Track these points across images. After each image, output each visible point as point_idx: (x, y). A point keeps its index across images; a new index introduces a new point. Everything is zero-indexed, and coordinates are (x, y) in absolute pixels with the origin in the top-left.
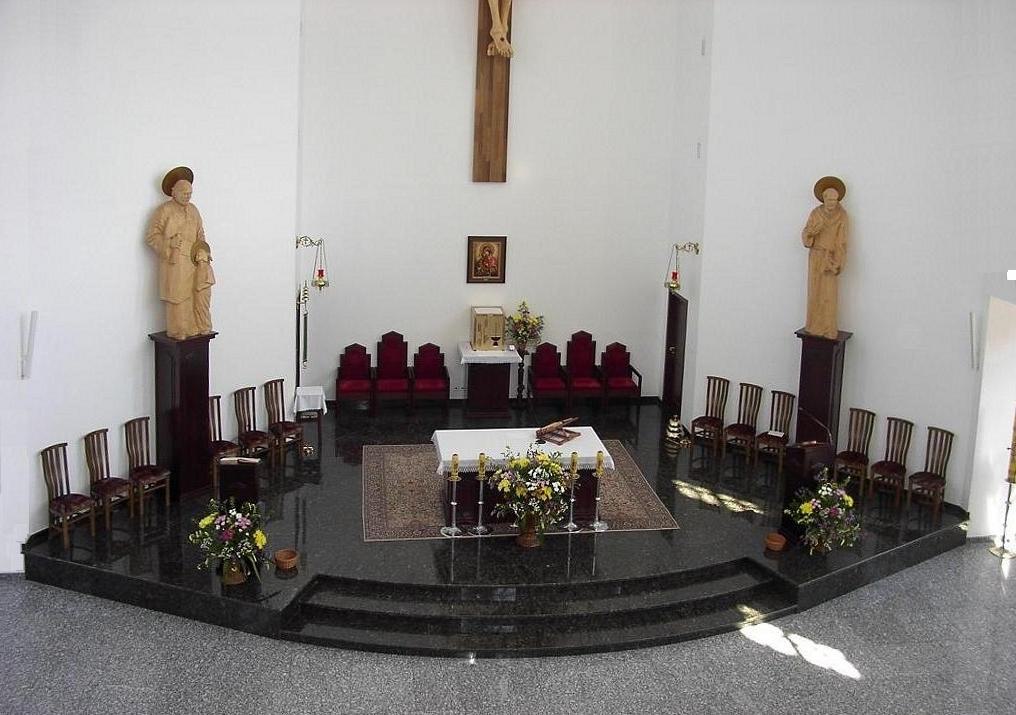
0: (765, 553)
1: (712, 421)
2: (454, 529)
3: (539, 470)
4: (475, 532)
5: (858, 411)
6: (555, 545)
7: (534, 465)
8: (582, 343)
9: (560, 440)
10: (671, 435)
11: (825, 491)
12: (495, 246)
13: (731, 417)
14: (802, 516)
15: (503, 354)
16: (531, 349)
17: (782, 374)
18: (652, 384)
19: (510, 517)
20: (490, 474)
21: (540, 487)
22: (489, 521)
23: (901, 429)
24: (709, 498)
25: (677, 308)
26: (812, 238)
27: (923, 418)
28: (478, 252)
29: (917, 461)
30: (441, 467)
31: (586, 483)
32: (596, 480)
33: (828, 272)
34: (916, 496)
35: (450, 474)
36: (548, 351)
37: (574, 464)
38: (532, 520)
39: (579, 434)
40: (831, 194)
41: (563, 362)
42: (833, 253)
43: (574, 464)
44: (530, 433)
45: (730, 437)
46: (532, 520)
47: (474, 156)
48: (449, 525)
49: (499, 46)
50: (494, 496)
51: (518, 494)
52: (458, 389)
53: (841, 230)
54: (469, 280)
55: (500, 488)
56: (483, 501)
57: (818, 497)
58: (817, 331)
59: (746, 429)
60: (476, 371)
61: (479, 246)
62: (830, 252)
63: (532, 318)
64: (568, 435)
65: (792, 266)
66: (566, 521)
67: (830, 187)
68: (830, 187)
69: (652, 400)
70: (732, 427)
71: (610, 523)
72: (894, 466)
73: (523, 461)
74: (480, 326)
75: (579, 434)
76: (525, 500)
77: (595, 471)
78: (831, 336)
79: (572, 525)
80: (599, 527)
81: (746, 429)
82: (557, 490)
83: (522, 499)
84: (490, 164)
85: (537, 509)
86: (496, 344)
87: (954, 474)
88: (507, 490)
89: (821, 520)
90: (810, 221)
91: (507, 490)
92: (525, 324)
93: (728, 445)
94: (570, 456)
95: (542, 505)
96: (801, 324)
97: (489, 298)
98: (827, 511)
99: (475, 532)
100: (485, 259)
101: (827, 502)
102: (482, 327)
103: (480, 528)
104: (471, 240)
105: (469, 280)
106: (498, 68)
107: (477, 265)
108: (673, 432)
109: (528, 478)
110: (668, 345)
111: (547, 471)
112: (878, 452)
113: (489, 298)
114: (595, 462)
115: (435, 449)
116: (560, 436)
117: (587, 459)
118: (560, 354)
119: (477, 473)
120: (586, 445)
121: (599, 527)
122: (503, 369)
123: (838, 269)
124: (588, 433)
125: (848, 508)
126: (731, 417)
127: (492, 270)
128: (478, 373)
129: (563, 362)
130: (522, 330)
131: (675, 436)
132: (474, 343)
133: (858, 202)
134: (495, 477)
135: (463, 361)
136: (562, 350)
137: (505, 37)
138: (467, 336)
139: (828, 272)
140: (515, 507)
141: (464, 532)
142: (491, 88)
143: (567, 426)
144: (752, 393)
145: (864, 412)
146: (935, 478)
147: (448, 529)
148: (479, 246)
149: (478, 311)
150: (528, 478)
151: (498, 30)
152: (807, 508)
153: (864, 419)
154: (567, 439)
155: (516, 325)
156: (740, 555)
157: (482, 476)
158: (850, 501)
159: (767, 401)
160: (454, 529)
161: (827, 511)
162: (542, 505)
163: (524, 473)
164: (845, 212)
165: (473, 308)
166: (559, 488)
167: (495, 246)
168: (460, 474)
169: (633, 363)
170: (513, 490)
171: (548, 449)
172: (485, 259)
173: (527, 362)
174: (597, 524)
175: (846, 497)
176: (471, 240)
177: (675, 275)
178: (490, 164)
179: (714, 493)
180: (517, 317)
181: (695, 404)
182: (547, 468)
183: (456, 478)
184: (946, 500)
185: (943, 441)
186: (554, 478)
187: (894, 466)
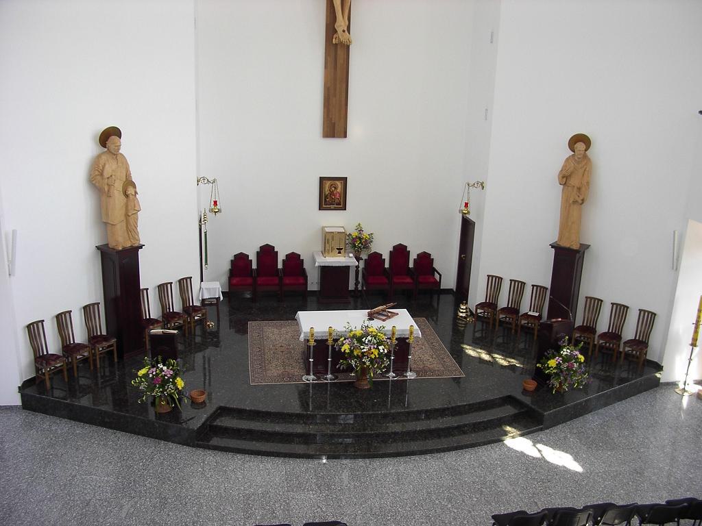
1: (490, 305)
2: (312, 377)
3: (369, 338)
4: (326, 379)
5: (591, 298)
7: (366, 335)
8: (400, 252)
9: (384, 318)
10: (461, 314)
11: (565, 352)
12: (339, 184)
13: (503, 302)
14: (549, 368)
16: (364, 256)
17: (539, 273)
18: (449, 280)
19: (350, 369)
20: (336, 340)
21: (370, 349)
23: (620, 310)
25: (467, 227)
26: (565, 178)
27: (635, 303)
28: (327, 188)
31: (402, 347)
33: (575, 202)
35: (308, 341)
36: (376, 257)
37: (393, 334)
38: (364, 371)
39: (397, 314)
40: (580, 146)
41: (387, 265)
42: (579, 189)
43: (393, 334)
45: (501, 316)
46: (364, 371)
47: (324, 118)
48: (308, 374)
49: (341, 36)
50: (338, 355)
51: (355, 353)
52: (313, 283)
53: (586, 172)
55: (343, 350)
57: (561, 356)
59: (513, 310)
60: (326, 271)
61: (327, 184)
63: (365, 235)
64: (389, 314)
65: (551, 197)
67: (581, 141)
68: (581, 141)
69: (448, 291)
70: (503, 309)
71: (418, 373)
72: (614, 336)
73: (359, 332)
74: (328, 240)
75: (397, 314)
76: (360, 358)
77: (408, 338)
78: (575, 247)
79: (392, 374)
80: (410, 375)
81: (513, 310)
82: (382, 351)
85: (368, 363)
86: (339, 253)
87: (655, 341)
88: (347, 351)
91: (347, 351)
92: (360, 239)
95: (372, 361)
96: (554, 238)
97: (334, 220)
99: (326, 379)
100: (332, 193)
101: (567, 359)
102: (330, 241)
104: (322, 180)
106: (340, 52)
107: (326, 197)
108: (462, 312)
109: (362, 343)
111: (375, 338)
112: (603, 326)
113: (334, 220)
114: (408, 332)
115: (298, 324)
117: (403, 330)
119: (327, 340)
120: (402, 322)
121: (410, 375)
122: (346, 269)
124: (403, 313)
125: (580, 363)
126: (503, 302)
127: (337, 201)
128: (332, 275)
129: (387, 265)
130: (358, 243)
131: (464, 315)
133: (599, 153)
134: (340, 343)
135: (317, 264)
136: (386, 256)
137: (346, 29)
138: (320, 247)
139: (575, 202)
140: (353, 363)
141: (319, 378)
144: (518, 286)
146: (641, 343)
147: (307, 377)
148: (327, 184)
149: (327, 230)
150: (362, 343)
151: (341, 24)
152: (552, 363)
153: (595, 304)
154: (389, 317)
155: (354, 240)
157: (330, 342)
158: (582, 358)
159: (528, 291)
160: (312, 377)
162: (372, 361)
163: (359, 340)
164: (589, 159)
165: (323, 228)
166: (383, 350)
168: (315, 341)
170: (352, 351)
172: (332, 193)
174: (409, 374)
175: (580, 356)
176: (322, 180)
177: (466, 205)
180: (355, 234)
181: (478, 293)
182: (375, 337)
183: (312, 343)
184: (648, 358)
185: (648, 319)
187: (614, 336)
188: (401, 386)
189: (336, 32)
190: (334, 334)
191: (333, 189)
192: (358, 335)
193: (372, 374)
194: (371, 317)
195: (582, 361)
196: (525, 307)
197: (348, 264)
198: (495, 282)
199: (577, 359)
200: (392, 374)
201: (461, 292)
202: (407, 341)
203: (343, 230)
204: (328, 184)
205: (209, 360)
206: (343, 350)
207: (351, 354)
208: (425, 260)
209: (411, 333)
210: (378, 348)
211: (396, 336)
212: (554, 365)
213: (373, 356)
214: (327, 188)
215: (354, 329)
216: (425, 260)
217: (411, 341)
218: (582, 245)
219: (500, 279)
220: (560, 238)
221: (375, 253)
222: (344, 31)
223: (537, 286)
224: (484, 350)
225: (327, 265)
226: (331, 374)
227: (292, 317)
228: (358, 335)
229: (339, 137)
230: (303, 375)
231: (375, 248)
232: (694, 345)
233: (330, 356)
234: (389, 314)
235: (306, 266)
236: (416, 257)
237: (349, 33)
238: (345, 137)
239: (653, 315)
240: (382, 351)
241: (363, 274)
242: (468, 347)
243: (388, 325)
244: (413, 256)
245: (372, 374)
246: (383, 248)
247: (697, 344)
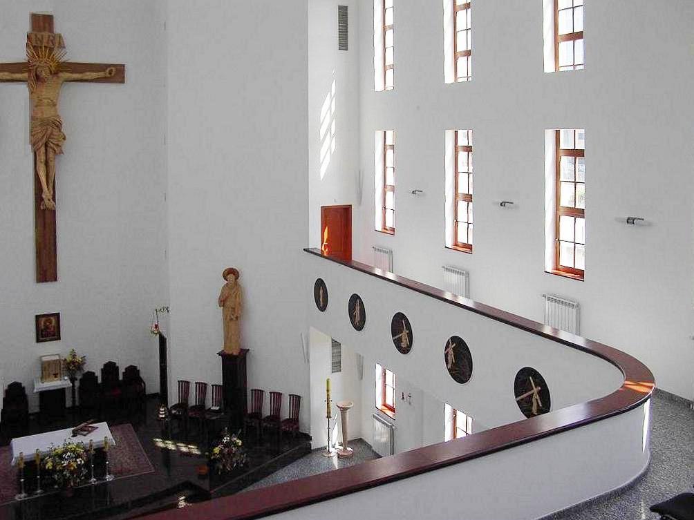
0: (199, 478)
1: (182, 405)
2: (23, 495)
3: (69, 454)
6: (78, 492)
7: (65, 452)
8: (110, 368)
9: (85, 433)
10: (161, 416)
11: (225, 440)
12: (53, 320)
13: (192, 401)
14: (214, 454)
15: (62, 382)
16: (79, 377)
17: (213, 375)
18: (153, 386)
19: (55, 482)
20: (42, 460)
21: (69, 463)
22: (44, 487)
23: (277, 396)
24: (184, 449)
26: (223, 302)
27: (286, 390)
28: (42, 323)
29: (285, 413)
31: (98, 456)
32: (105, 452)
34: (285, 432)
36: (91, 375)
37: (91, 446)
38: (67, 481)
40: (231, 277)
41: (100, 381)
42: (233, 309)
43: (91, 446)
44: (68, 432)
45: (190, 414)
46: (67, 481)
48: (20, 493)
49: (48, 203)
52: (34, 406)
54: (38, 341)
55: (47, 467)
56: (40, 475)
57: (222, 443)
58: (228, 352)
59: (201, 407)
60: (43, 394)
61: (43, 321)
63: (78, 359)
64: (90, 429)
65: (216, 314)
66: (88, 477)
67: (231, 273)
69: (154, 395)
70: (192, 407)
71: (115, 474)
72: (275, 417)
73: (60, 451)
74: (45, 368)
76: (61, 471)
79: (93, 479)
80: (109, 478)
81: (201, 407)
82: (79, 463)
84: (46, 270)
85: (68, 475)
86: (56, 377)
87: (303, 416)
89: (224, 455)
93: (190, 418)
94: (103, 439)
96: (220, 348)
97: (52, 350)
98: (227, 450)
100: (47, 327)
101: (227, 445)
102: (48, 369)
104: (37, 317)
105: (38, 341)
106: (48, 214)
107: (42, 331)
108: (162, 414)
111: (74, 454)
112: (267, 411)
114: (103, 443)
115: (11, 449)
116: (85, 431)
118: (97, 377)
119: (35, 461)
120: (101, 433)
121: (109, 478)
122: (61, 391)
124: (103, 426)
125: (238, 447)
127: (52, 333)
130: (72, 366)
131: (163, 416)
133: (246, 279)
134: (44, 461)
135: (35, 391)
136: (98, 374)
137: (51, 198)
138: (39, 374)
141: (29, 495)
142: (45, 227)
143: (91, 423)
144: (202, 387)
145: (258, 390)
146: (295, 420)
148: (43, 321)
149: (44, 359)
151: (46, 194)
152: (217, 450)
153: (259, 394)
154: (90, 432)
156: (184, 479)
157: (38, 462)
158: (240, 442)
159: (209, 390)
160: (23, 495)
161: (227, 450)
162: (72, 473)
163: (60, 456)
164: (240, 285)
166: (81, 461)
167: (53, 320)
168: (25, 463)
169: (141, 375)
172: (47, 327)
174: (108, 477)
175: (238, 441)
176: (37, 317)
178: (46, 270)
180: (69, 359)
181: (174, 398)
182: (73, 452)
185: (296, 400)
186: (78, 456)
187: (275, 417)
188: (103, 489)
190: (40, 454)
191: (48, 324)
193: (72, 484)
194: (75, 434)
195: (240, 444)
196: (211, 404)
197: (63, 387)
198: (185, 385)
199: (235, 444)
200: (93, 479)
201: (163, 396)
202: (104, 450)
203: (57, 358)
204: (43, 319)
205: (305, 361)
206: (47, 467)
207: (54, 470)
208: (132, 372)
210: (76, 461)
214: (42, 323)
215: (57, 448)
216: (132, 372)
218: (242, 350)
227: (7, 443)
231: (86, 369)
232: (329, 417)
234: (90, 429)
235: (27, 392)
236: (124, 371)
239: (299, 397)
241: (79, 392)
246: (95, 366)
247: (331, 416)
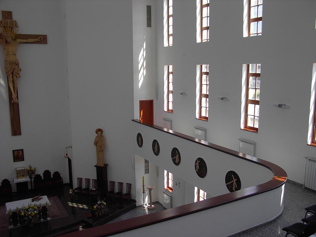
1: (80, 188)
2: (12, 226)
3: (31, 209)
4: (18, 226)
5: (111, 182)
7: (29, 208)
8: (47, 173)
11: (99, 202)
12: (20, 152)
13: (84, 186)
16: (33, 176)
17: (93, 175)
18: (66, 180)
19: (25, 221)
20: (19, 211)
21: (31, 213)
23: (121, 184)
25: (70, 161)
26: (96, 143)
27: (125, 182)
29: (125, 191)
30: (7, 212)
31: (44, 210)
32: (47, 208)
33: (100, 151)
35: (10, 213)
36: (38, 176)
38: (30, 220)
39: (43, 198)
40: (99, 132)
41: (43, 178)
43: (40, 205)
46: (30, 220)
47: (12, 128)
48: (11, 225)
49: (15, 100)
50: (21, 217)
51: (26, 215)
52: (14, 189)
53: (102, 141)
54: (14, 161)
55: (22, 215)
57: (97, 204)
59: (87, 189)
60: (18, 184)
62: (100, 146)
63: (33, 169)
67: (99, 131)
68: (99, 131)
69: (67, 184)
71: (51, 217)
72: (120, 193)
73: (27, 207)
75: (43, 198)
76: (28, 216)
77: (46, 206)
78: (102, 166)
79: (42, 219)
80: (49, 219)
81: (87, 189)
82: (35, 213)
83: (27, 216)
84: (16, 130)
86: (23, 177)
87: (132, 192)
88: (23, 215)
90: (95, 140)
91: (23, 215)
92: (31, 170)
94: (45, 203)
95: (32, 217)
96: (95, 164)
97: (20, 165)
99: (18, 226)
100: (18, 155)
101: (100, 205)
102: (19, 173)
103: (19, 225)
104: (14, 151)
109: (28, 211)
110: (69, 170)
112: (117, 190)
113: (20, 165)
114: (46, 204)
115: (5, 207)
116: (38, 199)
117: (44, 204)
119: (16, 212)
120: (44, 200)
121: (49, 219)
122: (26, 183)
123: (102, 150)
125: (104, 205)
126: (84, 186)
128: (20, 185)
129: (43, 178)
130: (30, 172)
132: (17, 177)
135: (14, 183)
137: (16, 98)
138: (16, 176)
139: (100, 151)
140: (26, 218)
144: (88, 180)
146: (129, 194)
147: (11, 226)
148: (16, 152)
149: (18, 169)
150: (28, 211)
151: (14, 96)
152: (95, 207)
153: (113, 183)
154: (39, 200)
155: (29, 171)
157: (18, 212)
158: (105, 203)
159: (91, 182)
160: (12, 226)
162: (32, 217)
163: (27, 210)
164: (103, 136)
165: (16, 168)
167: (20, 152)
170: (25, 214)
171: (35, 203)
172: (18, 155)
173: (33, 180)
174: (48, 218)
175: (104, 203)
176: (14, 151)
177: (67, 154)
178: (16, 130)
179: (77, 204)
180: (29, 169)
181: (75, 185)
183: (11, 214)
184: (131, 198)
185: (129, 186)
186: (35, 210)
187: (120, 193)
189: (12, 99)
191: (18, 154)
192: (27, 208)
193: (33, 221)
194: (33, 201)
196: (92, 187)
198: (80, 180)
199: (103, 204)
200: (42, 219)
201: (71, 184)
203: (23, 168)
204: (16, 152)
208: (57, 174)
209: (47, 204)
210: (34, 212)
211: (11, 212)
212: (96, 208)
213: (33, 215)
216: (57, 174)
217: (47, 207)
219: (81, 179)
220: (97, 163)
221: (38, 175)
222: (15, 99)
223: (94, 180)
224: (81, 204)
225: (18, 182)
226: (13, 225)
227: (4, 205)
228: (27, 208)
229: (19, 135)
230: (9, 226)
231: (37, 173)
233: (41, 215)
235: (11, 183)
236: (53, 174)
237: (18, 99)
238: (21, 134)
240: (35, 213)
242: (80, 205)
243: (38, 203)
244: (52, 174)
245: (33, 221)
